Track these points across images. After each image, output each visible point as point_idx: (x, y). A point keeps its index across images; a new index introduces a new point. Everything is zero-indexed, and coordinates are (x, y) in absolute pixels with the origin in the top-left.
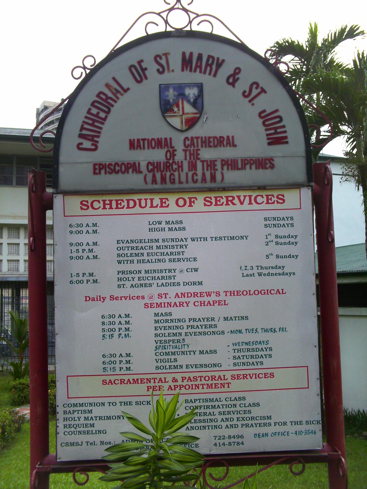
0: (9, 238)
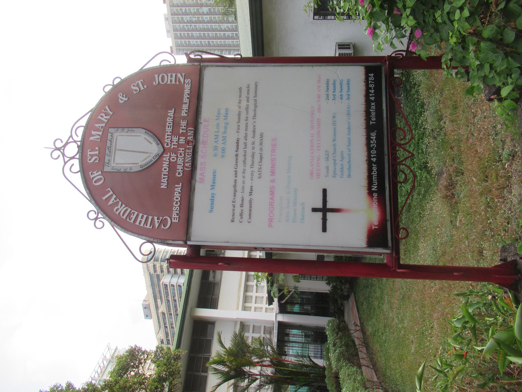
0: (249, 332)
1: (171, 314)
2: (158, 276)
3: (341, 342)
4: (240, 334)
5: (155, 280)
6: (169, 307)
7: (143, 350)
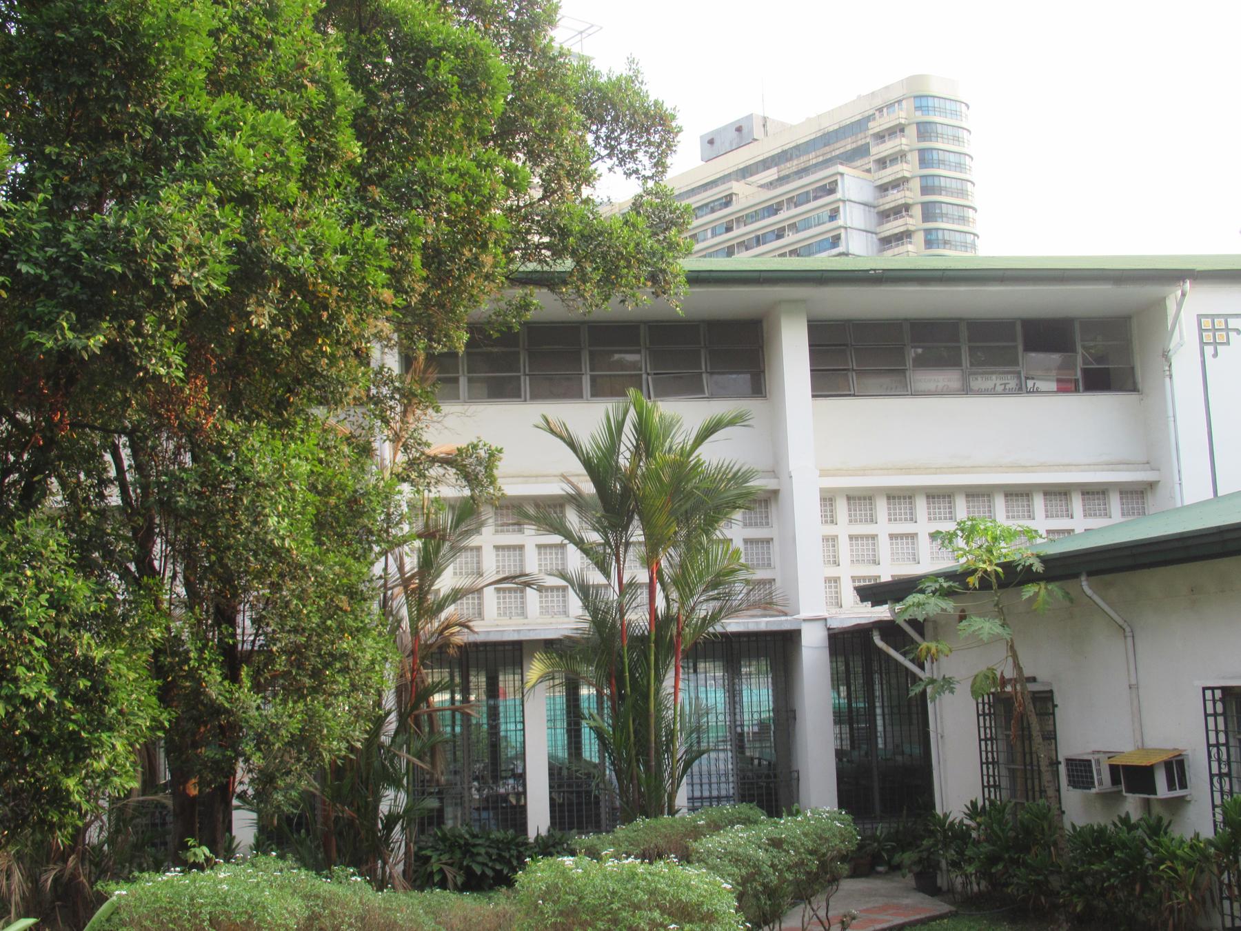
1: (729, 229)
2: (863, 151)
3: (789, 868)
4: (748, 494)
5: (848, 145)
6: (755, 216)
7: (669, 161)
